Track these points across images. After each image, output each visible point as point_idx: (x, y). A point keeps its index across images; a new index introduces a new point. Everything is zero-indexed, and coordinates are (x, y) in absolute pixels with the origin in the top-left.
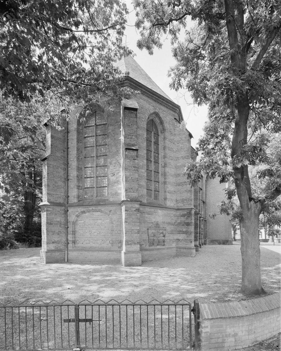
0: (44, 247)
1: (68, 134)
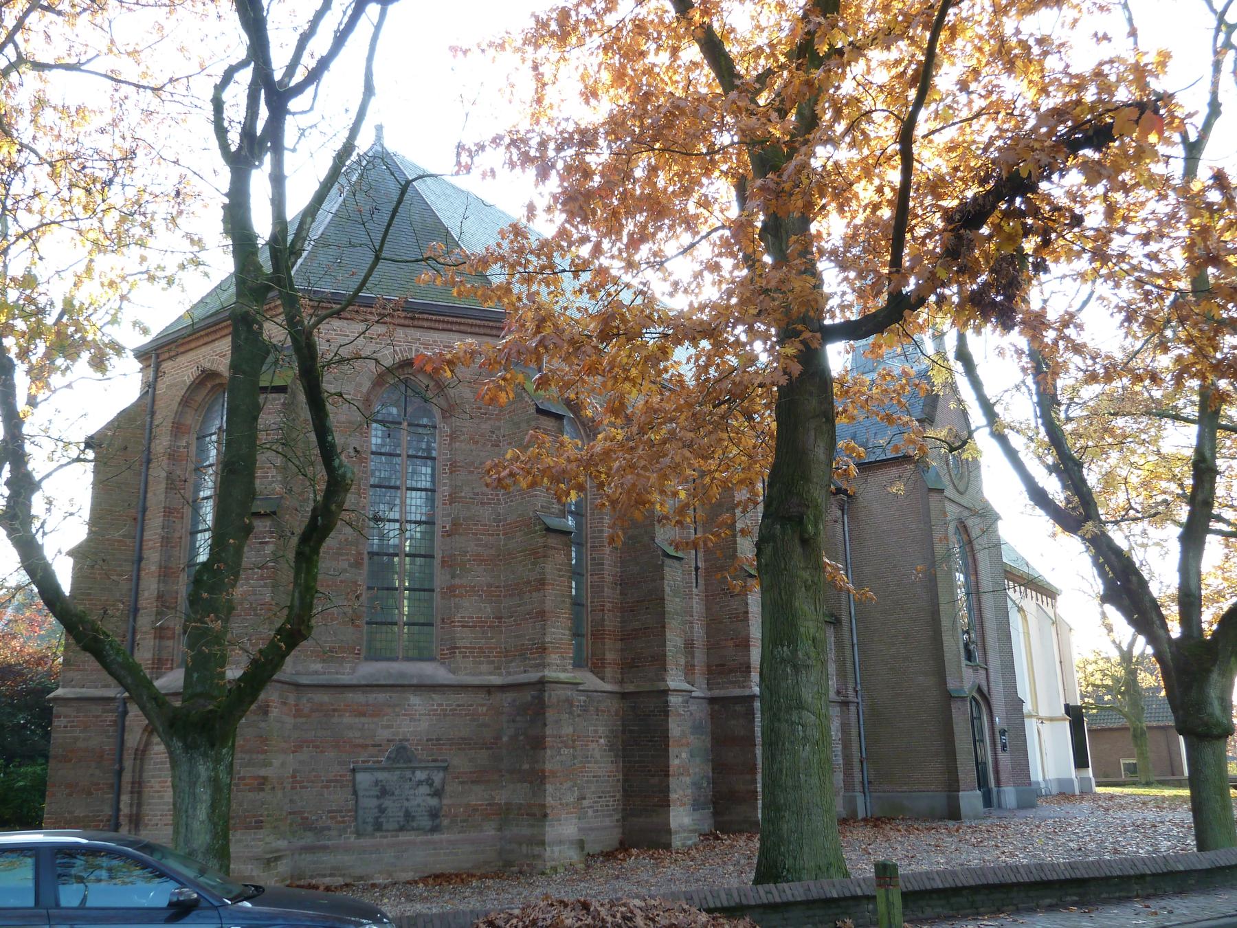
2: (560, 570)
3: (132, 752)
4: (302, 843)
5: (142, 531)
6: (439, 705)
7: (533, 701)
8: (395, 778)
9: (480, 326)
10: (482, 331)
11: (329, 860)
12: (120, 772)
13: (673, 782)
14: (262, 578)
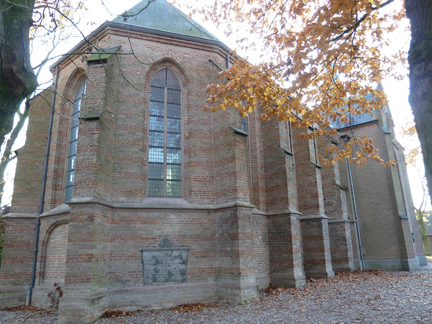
2: (242, 153)
3: (42, 242)
4: (116, 288)
6: (184, 219)
7: (231, 216)
8: (163, 255)
9: (200, 46)
10: (201, 48)
11: (129, 297)
12: (36, 252)
13: (294, 255)
14: (92, 151)
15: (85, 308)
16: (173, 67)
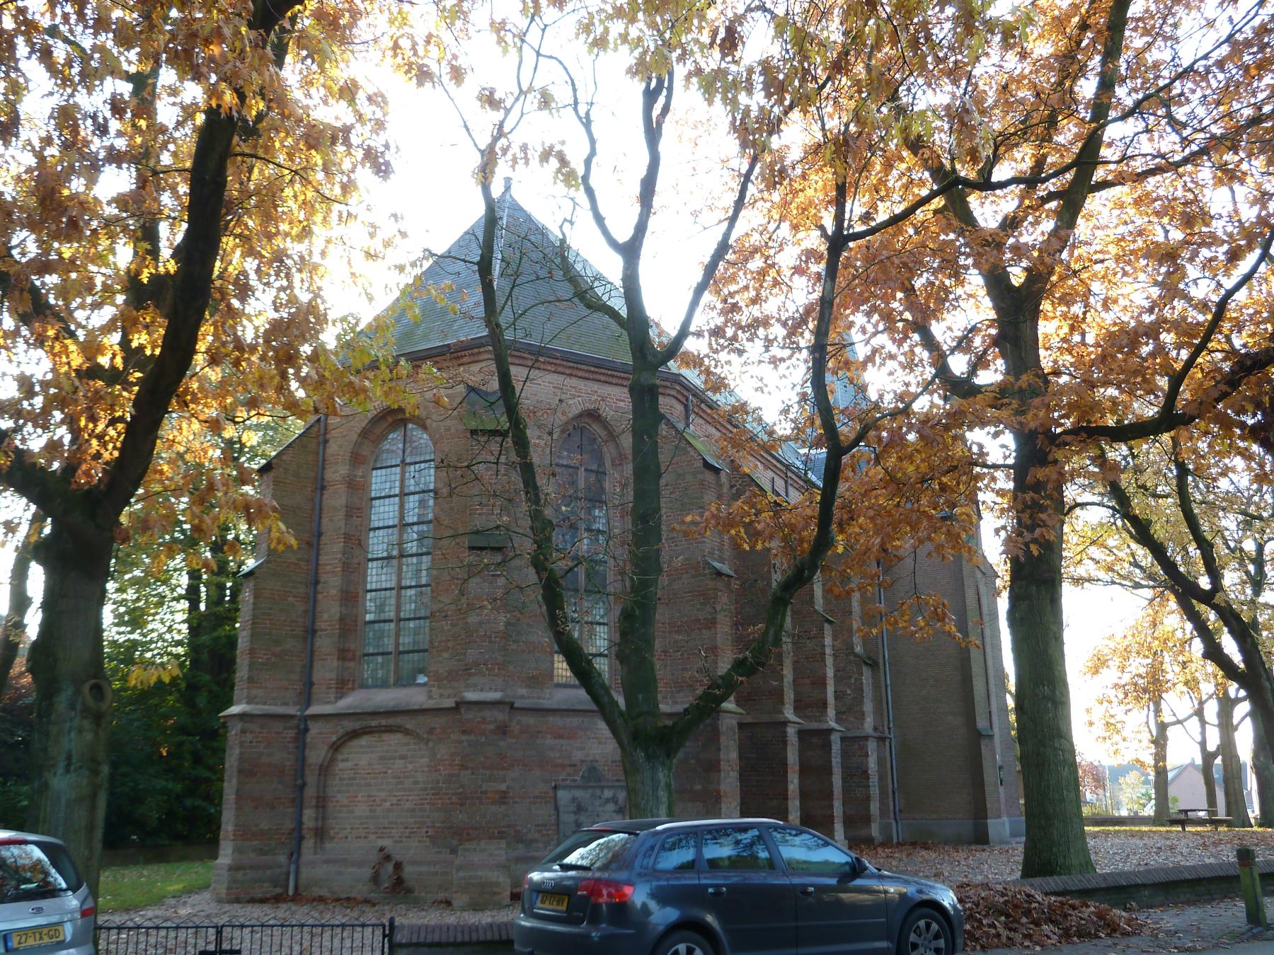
0: (226, 856)
1: (322, 495)
5: (318, 555)
15: (501, 880)
16: (595, 426)
